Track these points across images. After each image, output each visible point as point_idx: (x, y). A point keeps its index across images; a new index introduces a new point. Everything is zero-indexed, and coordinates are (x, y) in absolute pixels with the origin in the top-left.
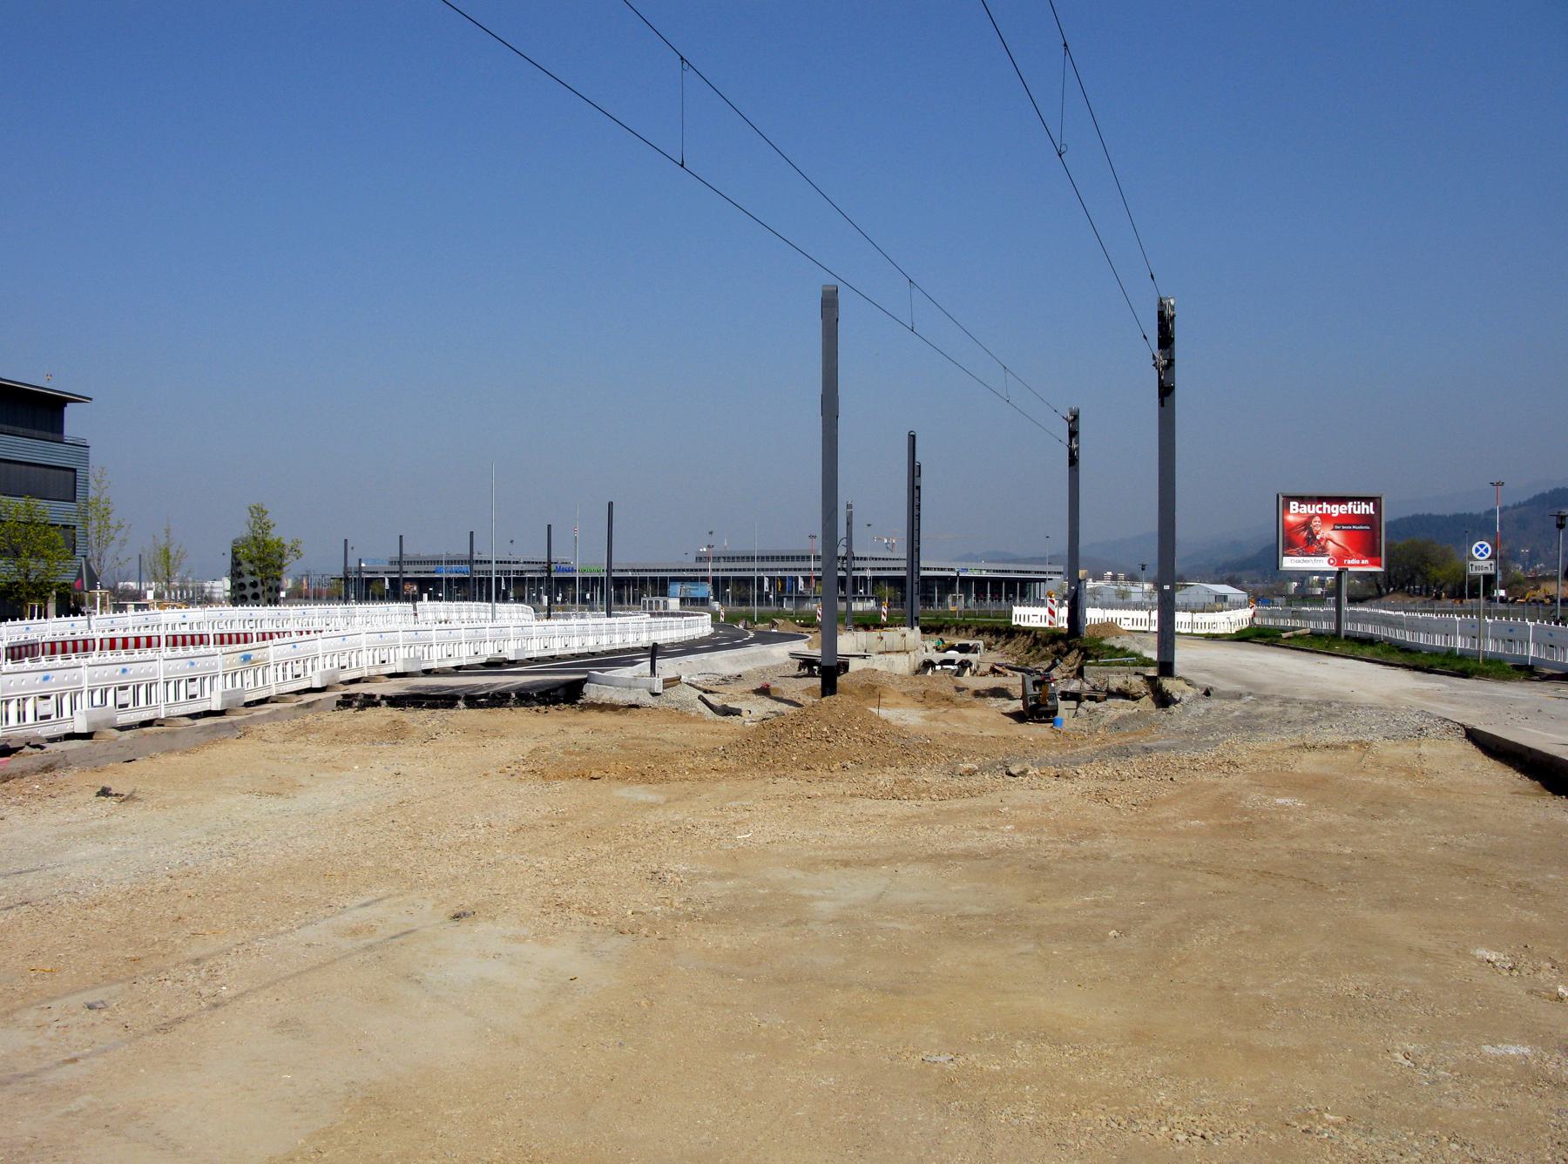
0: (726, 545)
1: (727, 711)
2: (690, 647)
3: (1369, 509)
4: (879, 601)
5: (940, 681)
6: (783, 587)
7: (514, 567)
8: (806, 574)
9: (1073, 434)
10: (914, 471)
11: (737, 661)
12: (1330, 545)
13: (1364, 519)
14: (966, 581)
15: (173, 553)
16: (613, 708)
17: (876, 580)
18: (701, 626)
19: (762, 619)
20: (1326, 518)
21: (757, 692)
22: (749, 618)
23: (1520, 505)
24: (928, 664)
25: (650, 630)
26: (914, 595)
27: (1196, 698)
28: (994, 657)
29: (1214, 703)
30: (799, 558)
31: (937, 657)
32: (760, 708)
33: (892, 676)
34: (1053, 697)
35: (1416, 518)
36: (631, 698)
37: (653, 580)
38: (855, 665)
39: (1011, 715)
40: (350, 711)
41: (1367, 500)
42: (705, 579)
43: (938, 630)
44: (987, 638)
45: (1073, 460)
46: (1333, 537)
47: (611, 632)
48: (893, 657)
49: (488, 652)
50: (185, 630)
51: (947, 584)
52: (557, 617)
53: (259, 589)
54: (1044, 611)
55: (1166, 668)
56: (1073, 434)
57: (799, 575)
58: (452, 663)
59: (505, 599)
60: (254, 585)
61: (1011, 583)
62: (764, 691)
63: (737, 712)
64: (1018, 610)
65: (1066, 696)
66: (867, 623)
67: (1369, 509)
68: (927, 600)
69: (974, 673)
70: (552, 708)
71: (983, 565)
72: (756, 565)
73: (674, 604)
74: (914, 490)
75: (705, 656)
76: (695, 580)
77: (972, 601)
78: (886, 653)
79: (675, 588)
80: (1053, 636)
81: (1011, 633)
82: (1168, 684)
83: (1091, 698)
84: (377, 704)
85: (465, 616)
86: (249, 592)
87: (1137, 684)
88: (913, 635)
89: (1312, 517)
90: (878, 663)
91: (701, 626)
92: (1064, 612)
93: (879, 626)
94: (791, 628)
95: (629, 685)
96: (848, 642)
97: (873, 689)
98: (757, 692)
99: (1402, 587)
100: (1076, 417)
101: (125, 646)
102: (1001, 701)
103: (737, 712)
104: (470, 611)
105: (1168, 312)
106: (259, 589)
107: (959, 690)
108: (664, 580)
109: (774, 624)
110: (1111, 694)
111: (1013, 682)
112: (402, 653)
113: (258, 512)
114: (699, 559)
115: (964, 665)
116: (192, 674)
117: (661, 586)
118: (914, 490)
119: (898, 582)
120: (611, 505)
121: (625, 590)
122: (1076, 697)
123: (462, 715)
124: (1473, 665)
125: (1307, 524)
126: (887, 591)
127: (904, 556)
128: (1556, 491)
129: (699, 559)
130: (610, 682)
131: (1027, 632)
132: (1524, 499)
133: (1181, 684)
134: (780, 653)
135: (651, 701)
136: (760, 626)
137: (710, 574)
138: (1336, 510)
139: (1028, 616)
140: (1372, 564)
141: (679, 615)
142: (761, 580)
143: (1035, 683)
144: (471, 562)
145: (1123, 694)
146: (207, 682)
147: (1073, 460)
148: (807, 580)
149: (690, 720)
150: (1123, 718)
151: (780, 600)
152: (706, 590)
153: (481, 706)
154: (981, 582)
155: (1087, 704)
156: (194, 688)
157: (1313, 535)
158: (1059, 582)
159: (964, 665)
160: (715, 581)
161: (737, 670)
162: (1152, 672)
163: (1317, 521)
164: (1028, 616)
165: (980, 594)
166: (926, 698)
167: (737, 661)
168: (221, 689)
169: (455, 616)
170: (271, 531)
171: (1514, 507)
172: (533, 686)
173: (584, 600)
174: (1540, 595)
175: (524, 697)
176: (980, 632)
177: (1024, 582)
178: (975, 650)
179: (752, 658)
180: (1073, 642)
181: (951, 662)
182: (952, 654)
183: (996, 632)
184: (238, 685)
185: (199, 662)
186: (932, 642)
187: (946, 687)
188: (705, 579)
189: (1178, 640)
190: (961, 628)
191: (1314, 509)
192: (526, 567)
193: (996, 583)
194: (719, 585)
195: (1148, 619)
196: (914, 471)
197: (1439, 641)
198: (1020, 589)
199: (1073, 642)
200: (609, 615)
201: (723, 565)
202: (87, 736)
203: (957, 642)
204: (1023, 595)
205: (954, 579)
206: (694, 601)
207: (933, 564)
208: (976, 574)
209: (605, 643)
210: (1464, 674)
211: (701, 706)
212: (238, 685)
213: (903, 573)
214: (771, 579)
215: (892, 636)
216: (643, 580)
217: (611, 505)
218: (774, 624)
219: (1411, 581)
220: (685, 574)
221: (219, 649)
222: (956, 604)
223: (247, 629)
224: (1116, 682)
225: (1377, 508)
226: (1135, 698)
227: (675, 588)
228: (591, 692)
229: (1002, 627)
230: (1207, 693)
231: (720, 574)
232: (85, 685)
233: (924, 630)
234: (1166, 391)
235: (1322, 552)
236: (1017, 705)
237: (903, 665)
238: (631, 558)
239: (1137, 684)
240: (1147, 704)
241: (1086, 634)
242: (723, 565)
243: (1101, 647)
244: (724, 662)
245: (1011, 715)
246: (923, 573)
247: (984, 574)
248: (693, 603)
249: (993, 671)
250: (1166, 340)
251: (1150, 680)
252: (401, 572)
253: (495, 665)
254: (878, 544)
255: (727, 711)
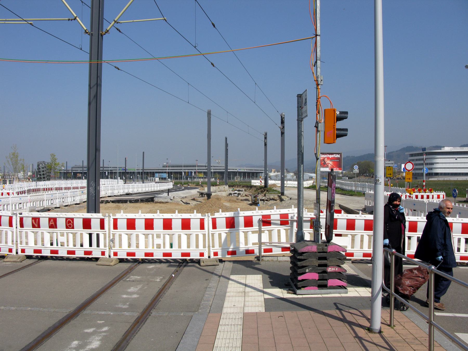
0: (171, 162)
1: (187, 203)
2: (169, 191)
3: (339, 156)
4: (215, 178)
5: (234, 197)
6: (188, 174)
7: (110, 169)
8: (195, 171)
9: (266, 138)
10: (227, 145)
11: (184, 193)
12: (329, 165)
13: (337, 158)
14: (240, 173)
15: (25, 166)
16: (163, 203)
17: (215, 172)
18: (170, 185)
19: (185, 184)
20: (328, 158)
21: (192, 200)
22: (181, 183)
23: (398, 151)
24: (230, 194)
25: (160, 186)
26: (226, 176)
27: (288, 200)
28: (247, 193)
29: (292, 201)
30: (193, 166)
31: (232, 192)
32: (194, 203)
33: (222, 196)
34: (258, 200)
35: (369, 154)
36: (166, 200)
37: (151, 172)
38: (213, 194)
39: (249, 204)
40: (103, 204)
41: (338, 154)
42: (165, 172)
43: (232, 186)
44: (245, 188)
45: (266, 145)
46: (330, 163)
47: (146, 187)
48: (222, 192)
49: (126, 191)
50: (45, 187)
51: (235, 174)
52: (128, 183)
53: (45, 176)
54: (259, 181)
55: (283, 194)
56: (266, 138)
57: (193, 171)
58: (119, 194)
59: (107, 178)
60: (44, 174)
61: (253, 173)
62: (194, 199)
63: (189, 204)
64: (253, 181)
65: (261, 200)
66: (214, 184)
67: (339, 156)
68: (230, 178)
69: (241, 196)
70: (149, 203)
71: (245, 168)
72: (183, 168)
73: (157, 179)
74: (227, 150)
75: (174, 193)
76: (163, 172)
77: (242, 178)
78: (221, 191)
79: (157, 175)
80: (261, 188)
81: (251, 187)
82: (283, 197)
83: (267, 200)
84: (109, 202)
85: (108, 183)
86: (42, 176)
87: (276, 197)
88: (227, 187)
89: (324, 158)
90: (219, 194)
91: (170, 185)
92: (263, 182)
93: (216, 185)
94: (193, 186)
95: (165, 198)
96: (213, 189)
97: (218, 199)
98: (192, 200)
99: (363, 174)
100: (266, 134)
101: (47, 190)
102: (247, 201)
103: (189, 204)
104: (107, 182)
105: (283, 116)
106: (45, 176)
107: (237, 199)
108: (153, 172)
109: (189, 185)
110: (271, 199)
111: (250, 198)
112: (110, 191)
113: (53, 155)
114: (164, 166)
115: (239, 194)
116: (20, 202)
117: (153, 174)
118: (227, 150)
119: (222, 173)
120: (143, 153)
121: (145, 175)
122: (263, 200)
123: (129, 204)
124: (353, 193)
125: (324, 160)
126: (218, 176)
127: (224, 165)
128: (408, 147)
129: (164, 166)
130: (161, 197)
131: (255, 186)
132: (399, 149)
133: (286, 197)
134: (194, 192)
135: (170, 201)
136: (185, 185)
137: (167, 171)
138: (331, 156)
139: (256, 182)
140: (340, 169)
141: (158, 183)
142: (192, 172)
143: (254, 197)
144: (82, 167)
145: (273, 199)
146: (25, 204)
147: (266, 145)
148: (195, 173)
149: (179, 205)
150: (272, 204)
151: (187, 178)
152: (166, 175)
153: (133, 203)
154: (244, 173)
155: (266, 202)
156: (21, 206)
157: (325, 162)
158: (263, 175)
159: (239, 194)
160: (168, 173)
161: (185, 196)
162: (280, 195)
163: (326, 159)
164: (256, 182)
165: (244, 176)
166: (230, 201)
167: (184, 193)
168: (29, 206)
169: (106, 183)
170: (57, 160)
171: (396, 151)
172: (145, 198)
173: (131, 179)
174: (400, 176)
175: (142, 201)
176: (243, 187)
177: (257, 173)
178: (242, 191)
179: (187, 193)
180: (265, 188)
181: (236, 193)
182: (236, 192)
183: (247, 187)
184: (35, 205)
185: (22, 198)
186: (231, 189)
187: (235, 199)
188: (165, 172)
189: (285, 188)
190: (239, 186)
191: (325, 156)
192: (113, 169)
193: (249, 173)
194: (170, 174)
195: (279, 183)
196: (227, 145)
197: (350, 188)
198: (255, 175)
199: (265, 188)
200: (143, 183)
201: (170, 168)
202: (59, 208)
203: (237, 189)
204: (256, 177)
205: (237, 172)
206: (162, 179)
207: (231, 168)
208: (243, 171)
209: (158, 189)
210: (351, 195)
211: (181, 202)
212: (35, 205)
213: (224, 171)
214: (185, 172)
215: (222, 187)
216: (148, 172)
217: (143, 153)
218: (189, 185)
219: (365, 173)
220: (160, 171)
221: (56, 192)
222: (237, 179)
223: (52, 187)
224: (272, 197)
225: (341, 156)
226: (276, 200)
227: (157, 175)
228: (156, 200)
229: (249, 185)
230: (291, 199)
231: (170, 171)
232: (10, 202)
233: (229, 186)
234: (283, 133)
235: (327, 167)
236: (251, 202)
237: (224, 194)
238: (149, 166)
239: (276, 197)
240: (278, 201)
241: (268, 187)
242: (170, 168)
243: (271, 190)
244: (181, 194)
245: (249, 204)
246: (229, 170)
247: (245, 171)
248: (163, 179)
249: (246, 195)
250: (283, 122)
251: (279, 196)
252: (83, 170)
253: (128, 194)
254: (218, 163)
255: (187, 203)
